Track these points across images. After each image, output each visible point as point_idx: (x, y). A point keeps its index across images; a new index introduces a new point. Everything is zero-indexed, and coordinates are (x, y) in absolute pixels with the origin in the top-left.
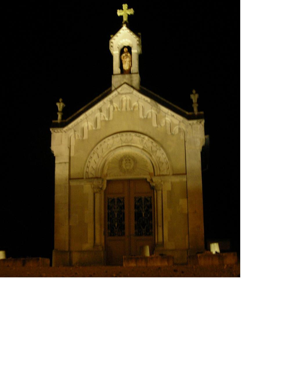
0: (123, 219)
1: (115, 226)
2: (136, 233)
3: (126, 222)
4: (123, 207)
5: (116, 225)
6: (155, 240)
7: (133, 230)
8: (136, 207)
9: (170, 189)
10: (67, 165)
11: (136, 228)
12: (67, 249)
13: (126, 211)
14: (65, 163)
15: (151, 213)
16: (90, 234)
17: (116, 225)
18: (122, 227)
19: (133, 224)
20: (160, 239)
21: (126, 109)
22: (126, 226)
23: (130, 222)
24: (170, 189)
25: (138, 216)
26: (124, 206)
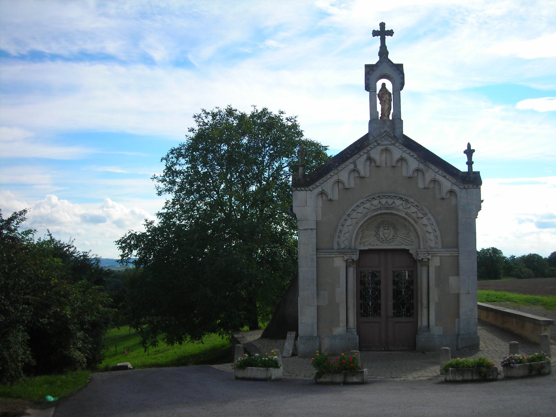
0: (378, 297)
1: (369, 305)
2: (394, 314)
3: (383, 302)
4: (378, 283)
5: (370, 304)
6: (417, 323)
7: (391, 312)
8: (395, 283)
9: (438, 264)
10: (315, 232)
11: (394, 309)
12: (315, 335)
13: (382, 287)
14: (312, 229)
15: (413, 290)
16: (343, 317)
17: (370, 304)
18: (377, 310)
19: (391, 303)
20: (425, 323)
21: (386, 163)
22: (383, 307)
23: (387, 301)
24: (438, 264)
25: (397, 293)
26: (379, 281)
